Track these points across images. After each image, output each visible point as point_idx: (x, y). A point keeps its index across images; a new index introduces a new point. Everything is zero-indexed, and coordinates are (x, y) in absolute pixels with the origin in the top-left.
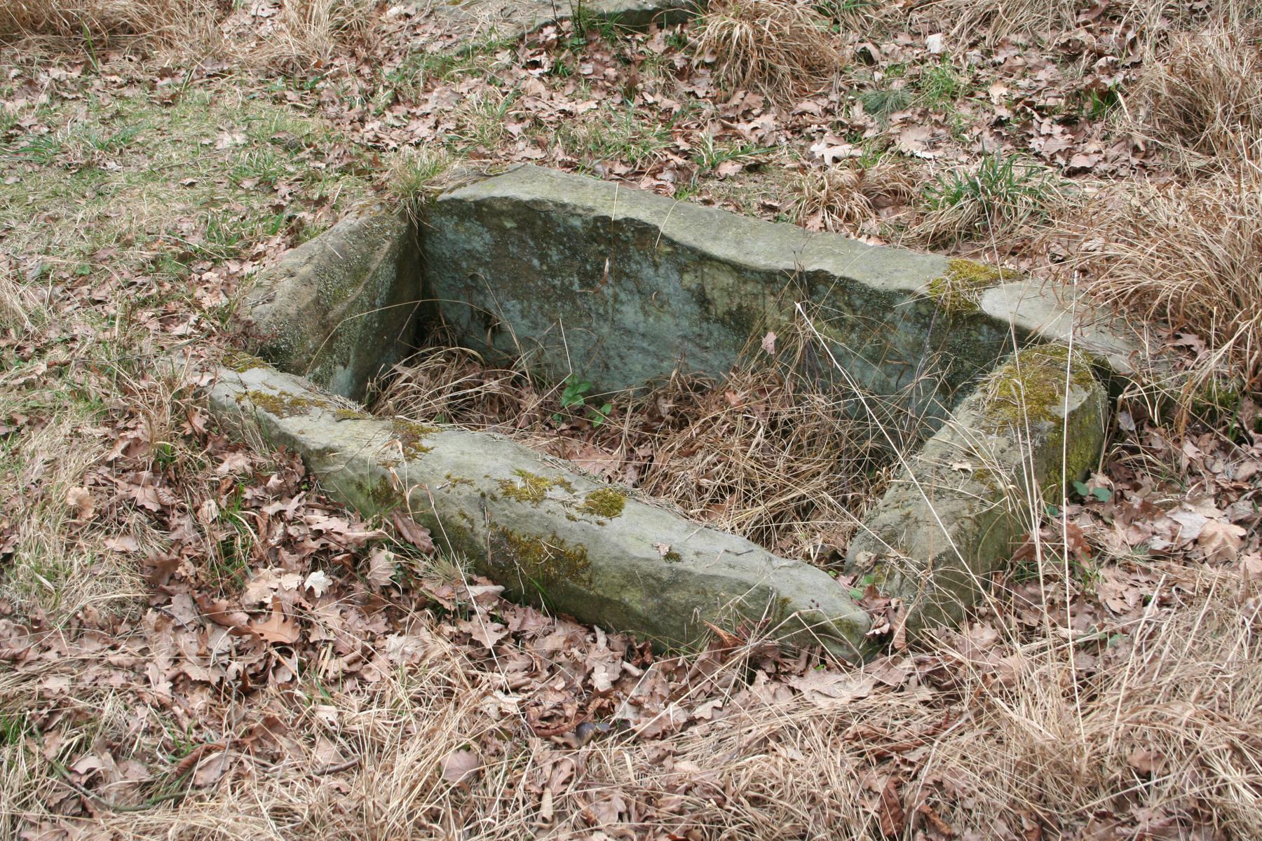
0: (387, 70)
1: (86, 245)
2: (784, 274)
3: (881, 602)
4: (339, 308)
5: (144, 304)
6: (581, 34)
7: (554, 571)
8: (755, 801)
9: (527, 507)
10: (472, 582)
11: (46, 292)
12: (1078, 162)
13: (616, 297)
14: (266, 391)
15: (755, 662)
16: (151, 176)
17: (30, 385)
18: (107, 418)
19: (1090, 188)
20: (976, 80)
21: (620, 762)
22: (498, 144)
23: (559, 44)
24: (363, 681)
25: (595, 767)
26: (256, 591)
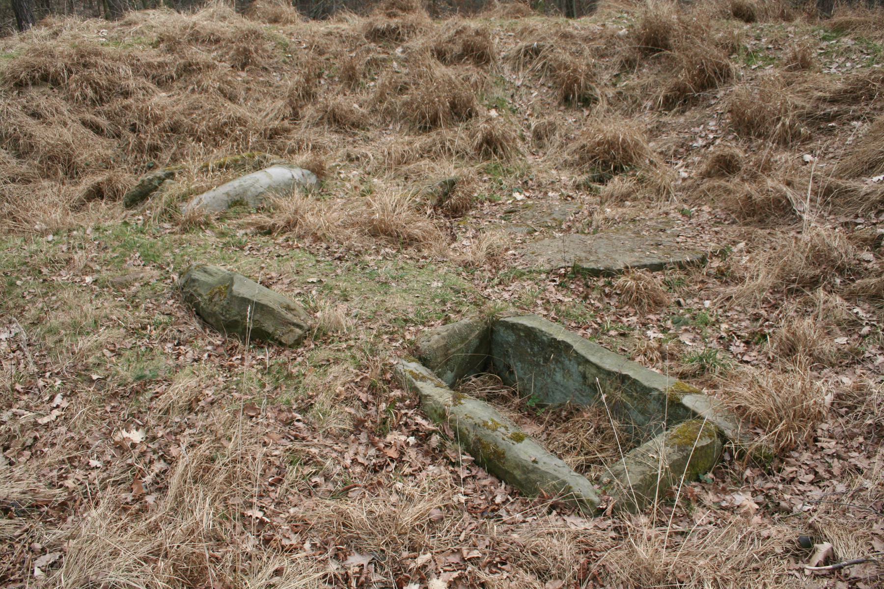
0: (500, 272)
1: (374, 309)
2: (614, 373)
3: (606, 497)
4: (453, 350)
5: (386, 333)
6: (573, 273)
7: (492, 457)
8: (534, 554)
9: (489, 432)
10: (463, 454)
11: (355, 321)
12: (746, 358)
13: (554, 369)
14: (415, 371)
15: (553, 507)
16: (405, 291)
17: (339, 350)
18: (359, 367)
19: (747, 368)
20: (717, 320)
21: (492, 528)
22: (532, 306)
23: (565, 275)
24: (415, 478)
25: (484, 528)
26: (389, 438)
